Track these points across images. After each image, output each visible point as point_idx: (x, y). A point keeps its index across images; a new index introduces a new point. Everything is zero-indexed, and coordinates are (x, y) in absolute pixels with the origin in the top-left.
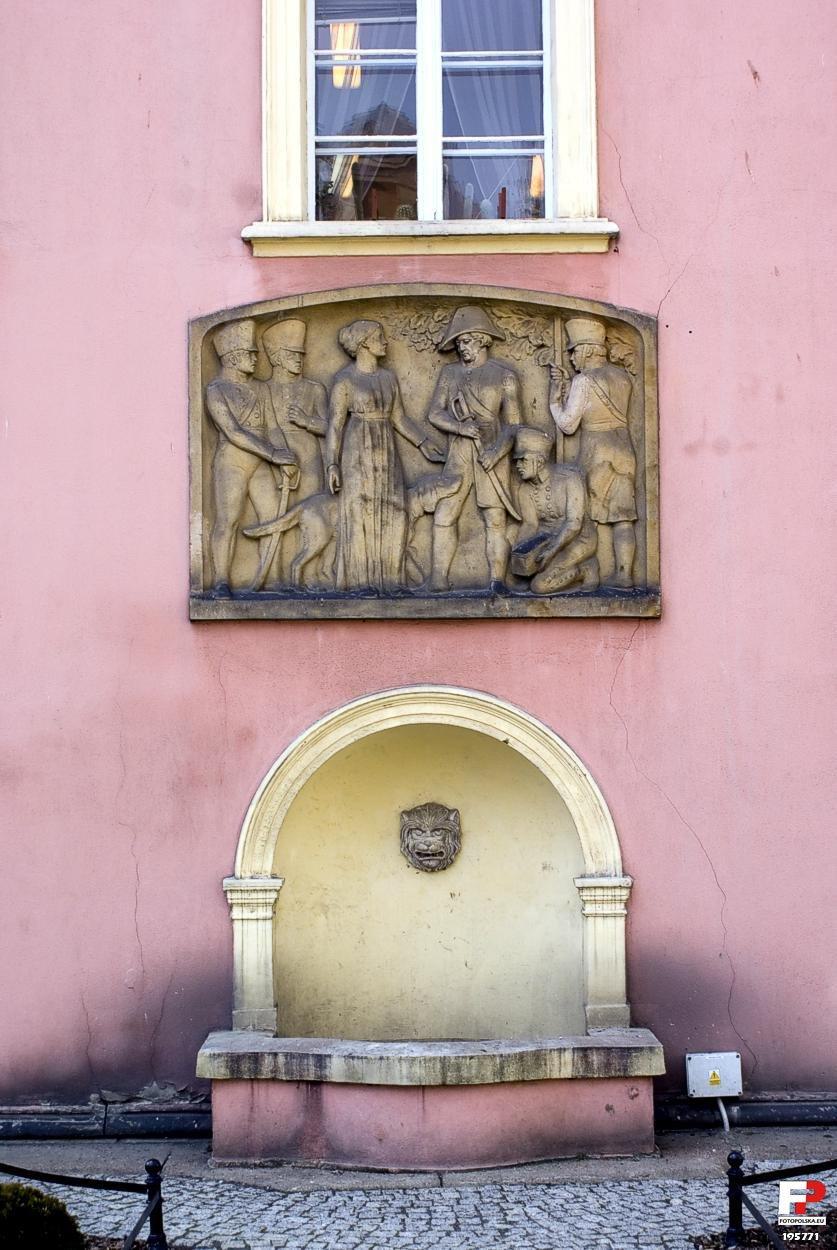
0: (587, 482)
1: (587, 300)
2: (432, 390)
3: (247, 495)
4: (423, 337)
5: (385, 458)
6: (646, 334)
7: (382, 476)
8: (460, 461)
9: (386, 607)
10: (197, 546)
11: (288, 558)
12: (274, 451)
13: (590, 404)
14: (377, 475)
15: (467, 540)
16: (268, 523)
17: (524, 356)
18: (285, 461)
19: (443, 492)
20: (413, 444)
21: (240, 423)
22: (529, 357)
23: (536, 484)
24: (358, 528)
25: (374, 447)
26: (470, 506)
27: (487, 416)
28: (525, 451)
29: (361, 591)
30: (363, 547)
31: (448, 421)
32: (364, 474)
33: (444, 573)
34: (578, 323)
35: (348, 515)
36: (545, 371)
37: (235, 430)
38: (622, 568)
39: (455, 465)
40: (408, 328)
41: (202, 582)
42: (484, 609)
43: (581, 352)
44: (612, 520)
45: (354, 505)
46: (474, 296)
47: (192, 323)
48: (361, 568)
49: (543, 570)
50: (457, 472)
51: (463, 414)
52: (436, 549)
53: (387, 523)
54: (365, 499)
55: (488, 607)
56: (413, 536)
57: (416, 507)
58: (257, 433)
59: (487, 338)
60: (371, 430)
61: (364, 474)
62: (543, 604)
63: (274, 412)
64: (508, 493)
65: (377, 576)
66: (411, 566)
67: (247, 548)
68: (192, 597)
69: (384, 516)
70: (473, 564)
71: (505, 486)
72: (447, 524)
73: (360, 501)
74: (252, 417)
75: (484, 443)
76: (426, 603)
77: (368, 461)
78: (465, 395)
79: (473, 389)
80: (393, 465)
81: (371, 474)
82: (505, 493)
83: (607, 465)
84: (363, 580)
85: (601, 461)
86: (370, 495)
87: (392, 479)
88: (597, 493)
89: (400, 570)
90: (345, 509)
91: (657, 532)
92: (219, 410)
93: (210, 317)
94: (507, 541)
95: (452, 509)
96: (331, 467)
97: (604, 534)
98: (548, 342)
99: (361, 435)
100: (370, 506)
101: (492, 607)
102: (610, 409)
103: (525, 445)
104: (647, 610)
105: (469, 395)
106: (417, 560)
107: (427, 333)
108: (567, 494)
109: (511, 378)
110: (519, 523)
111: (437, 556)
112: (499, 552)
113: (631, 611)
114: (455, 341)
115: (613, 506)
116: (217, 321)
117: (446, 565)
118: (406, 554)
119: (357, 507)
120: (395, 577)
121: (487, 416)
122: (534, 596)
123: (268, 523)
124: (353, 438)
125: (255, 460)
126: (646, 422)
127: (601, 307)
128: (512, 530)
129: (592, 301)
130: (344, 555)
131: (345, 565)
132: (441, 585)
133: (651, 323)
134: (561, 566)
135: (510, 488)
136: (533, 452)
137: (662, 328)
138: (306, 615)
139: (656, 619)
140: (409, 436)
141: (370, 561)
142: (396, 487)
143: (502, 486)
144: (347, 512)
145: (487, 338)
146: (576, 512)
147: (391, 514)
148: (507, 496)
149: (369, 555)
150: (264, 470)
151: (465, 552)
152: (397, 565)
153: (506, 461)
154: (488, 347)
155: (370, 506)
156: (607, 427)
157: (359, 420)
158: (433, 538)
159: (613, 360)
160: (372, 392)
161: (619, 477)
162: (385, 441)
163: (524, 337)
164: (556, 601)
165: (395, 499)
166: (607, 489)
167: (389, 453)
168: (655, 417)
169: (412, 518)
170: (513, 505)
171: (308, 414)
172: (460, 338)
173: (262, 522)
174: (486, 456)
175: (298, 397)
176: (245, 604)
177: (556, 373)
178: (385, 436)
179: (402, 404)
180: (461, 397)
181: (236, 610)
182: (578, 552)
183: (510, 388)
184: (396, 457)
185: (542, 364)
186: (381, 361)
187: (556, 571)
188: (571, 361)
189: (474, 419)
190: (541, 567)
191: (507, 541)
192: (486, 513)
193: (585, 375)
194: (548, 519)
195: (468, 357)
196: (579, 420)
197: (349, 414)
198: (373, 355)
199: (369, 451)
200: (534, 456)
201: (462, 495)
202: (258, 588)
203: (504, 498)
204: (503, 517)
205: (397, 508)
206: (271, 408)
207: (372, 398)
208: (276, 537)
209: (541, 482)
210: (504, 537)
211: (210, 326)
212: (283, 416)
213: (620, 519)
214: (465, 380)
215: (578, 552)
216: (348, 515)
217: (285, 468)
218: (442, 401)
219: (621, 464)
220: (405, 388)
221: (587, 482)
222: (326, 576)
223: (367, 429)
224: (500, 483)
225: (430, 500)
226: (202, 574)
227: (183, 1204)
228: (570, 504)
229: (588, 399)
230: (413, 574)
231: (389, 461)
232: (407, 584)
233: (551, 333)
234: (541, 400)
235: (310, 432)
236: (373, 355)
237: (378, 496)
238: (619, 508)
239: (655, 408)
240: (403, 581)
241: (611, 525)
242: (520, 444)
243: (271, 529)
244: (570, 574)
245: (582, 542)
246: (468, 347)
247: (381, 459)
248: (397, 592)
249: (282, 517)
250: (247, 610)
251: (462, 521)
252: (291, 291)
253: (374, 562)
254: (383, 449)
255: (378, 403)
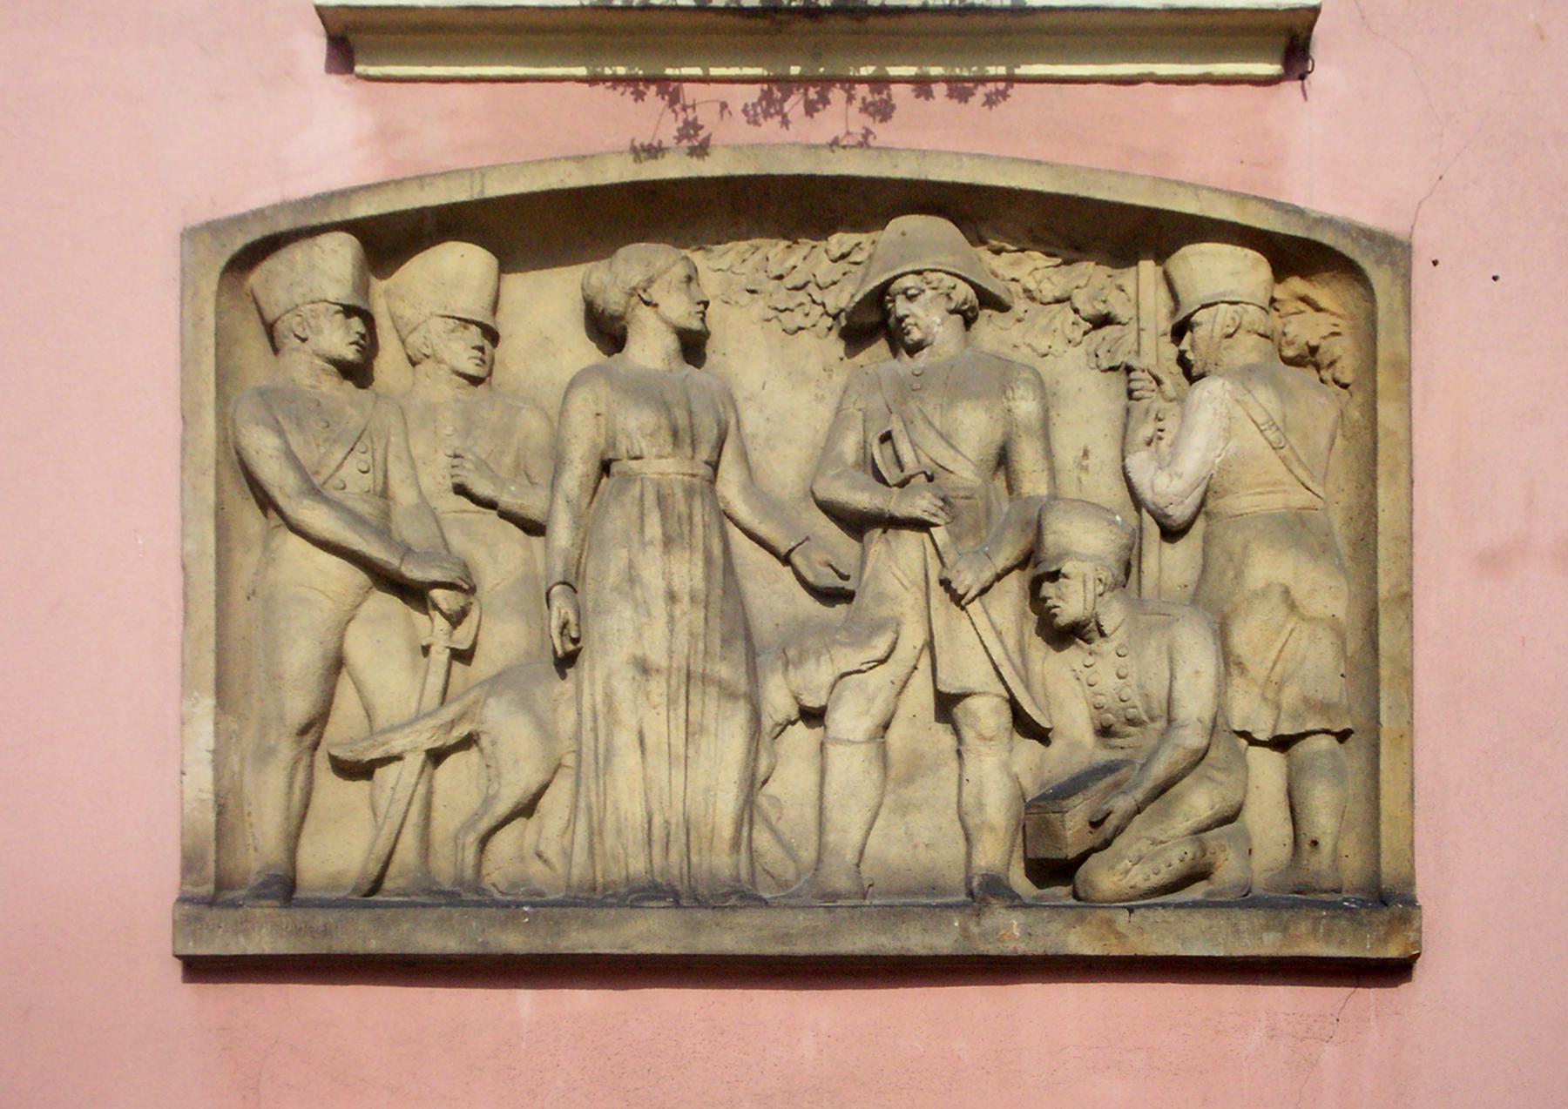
0: (1222, 635)
1: (1232, 194)
2: (823, 428)
3: (337, 663)
4: (801, 296)
5: (699, 571)
6: (1380, 278)
7: (690, 617)
8: (891, 585)
9: (696, 928)
10: (201, 780)
11: (446, 821)
12: (407, 551)
13: (1232, 446)
14: (677, 613)
15: (909, 779)
16: (393, 729)
17: (1059, 346)
18: (435, 575)
19: (850, 659)
20: (772, 550)
21: (317, 480)
22: (1071, 350)
23: (1088, 641)
24: (625, 740)
25: (668, 542)
26: (920, 697)
27: (965, 471)
28: (1062, 556)
29: (631, 892)
30: (639, 785)
31: (863, 490)
32: (641, 606)
33: (850, 856)
34: (1202, 253)
35: (600, 707)
36: (1117, 382)
37: (302, 494)
38: (1315, 843)
39: (881, 597)
40: (762, 275)
41: (211, 867)
42: (954, 936)
43: (1209, 325)
44: (1286, 729)
45: (615, 682)
46: (932, 177)
47: (191, 235)
48: (635, 835)
49: (1107, 844)
50: (885, 611)
51: (901, 467)
52: (831, 798)
53: (702, 730)
54: (644, 668)
55: (964, 929)
56: (772, 769)
57: (778, 700)
58: (365, 509)
59: (964, 292)
60: (661, 500)
61: (641, 606)
62: (1110, 923)
63: (414, 467)
64: (1018, 662)
65: (674, 857)
66: (763, 839)
67: (332, 790)
68: (182, 900)
69: (695, 711)
70: (925, 836)
71: (1011, 642)
72: (860, 735)
73: (630, 672)
74: (351, 470)
75: (956, 538)
76: (802, 919)
77: (652, 570)
78: (907, 423)
79: (929, 409)
80: (718, 591)
81: (659, 608)
82: (1010, 659)
83: (1276, 597)
84: (638, 866)
85: (1261, 584)
86: (657, 657)
87: (716, 623)
88: (1248, 665)
89: (735, 845)
90: (593, 694)
91: (1406, 756)
92: (263, 448)
93: (240, 221)
94: (1015, 779)
95: (871, 700)
96: (556, 589)
97: (1267, 768)
98: (1121, 311)
99: (635, 511)
100: (657, 687)
101: (974, 929)
102: (1283, 459)
103: (1064, 541)
104: (1384, 941)
105: (919, 423)
106: (781, 826)
107: (812, 288)
108: (1171, 661)
109: (1027, 381)
110: (1041, 735)
111: (835, 815)
112: (996, 808)
113: (1342, 942)
114: (881, 295)
115: (1290, 695)
116: (256, 233)
117: (855, 836)
118: (749, 808)
119: (624, 688)
120: (721, 862)
121: (965, 471)
122: (1085, 900)
123: (393, 729)
124: (617, 519)
125: (360, 577)
126: (1381, 492)
127: (1266, 210)
128: (1028, 749)
129: (1244, 198)
130: (589, 808)
131: (591, 833)
132: (842, 883)
133: (1395, 250)
134: (1155, 832)
135: (1022, 651)
136: (1081, 558)
137: (1420, 267)
138: (485, 944)
139: (1396, 971)
140: (763, 530)
141: (658, 820)
142: (726, 642)
143: (1002, 642)
144: (599, 698)
145: (964, 292)
146: (1194, 704)
147: (712, 707)
148: (1013, 666)
149: (655, 806)
150: (385, 603)
151: (904, 809)
152: (727, 832)
153: (1014, 585)
154: (969, 320)
155: (657, 687)
156: (1275, 502)
157: (628, 478)
158: (823, 773)
159: (1290, 352)
160: (665, 407)
161: (1304, 625)
162: (699, 530)
163: (1058, 301)
164: (1145, 918)
165: (723, 671)
166: (1273, 655)
167: (708, 560)
168: (1403, 477)
169: (767, 723)
170: (1028, 687)
171: (503, 474)
172: (896, 286)
173: (377, 728)
174: (961, 565)
175: (476, 433)
176: (320, 919)
177: (1142, 382)
178: (698, 519)
179: (744, 456)
180: (896, 427)
181: (298, 932)
182: (1199, 802)
183: (1026, 406)
184: (726, 572)
185: (1105, 365)
186: (692, 346)
187: (1143, 846)
188: (1182, 355)
189: (930, 479)
190: (1104, 833)
191: (1015, 779)
192: (958, 711)
193: (1221, 376)
194: (1117, 727)
195: (916, 335)
196: (1201, 489)
197: (605, 467)
198: (667, 322)
199: (656, 551)
200: (1087, 567)
201: (895, 669)
202: (366, 888)
203: (1006, 671)
204: (1006, 716)
205: (728, 693)
206: (404, 455)
207: (664, 422)
208: (415, 761)
209: (1102, 634)
210: (1006, 767)
211: (239, 242)
212: (436, 479)
213: (1310, 726)
214: (909, 389)
215: (1199, 802)
216: (600, 707)
217: (438, 594)
218: (849, 446)
219: (1313, 592)
220: (751, 419)
221: (1222, 635)
222: (546, 862)
223: (650, 499)
224: (999, 634)
225: (814, 681)
226: (212, 847)
227: (1336, 382)
228: (1180, 684)
229: (1228, 433)
230: (769, 858)
231: (708, 577)
232: (753, 882)
233: (1130, 289)
234: (1105, 452)
235: (506, 515)
236: (667, 322)
237: (680, 661)
238: (1306, 700)
239: (1402, 455)
240: (744, 874)
241: (1281, 744)
242: (1049, 539)
243: (397, 744)
244: (1176, 859)
245: (1211, 779)
246: (914, 308)
247: (688, 572)
248: (727, 896)
249: (429, 715)
250: (326, 931)
251: (895, 735)
252: (449, 163)
253: (667, 822)
254: (691, 547)
255: (679, 437)
